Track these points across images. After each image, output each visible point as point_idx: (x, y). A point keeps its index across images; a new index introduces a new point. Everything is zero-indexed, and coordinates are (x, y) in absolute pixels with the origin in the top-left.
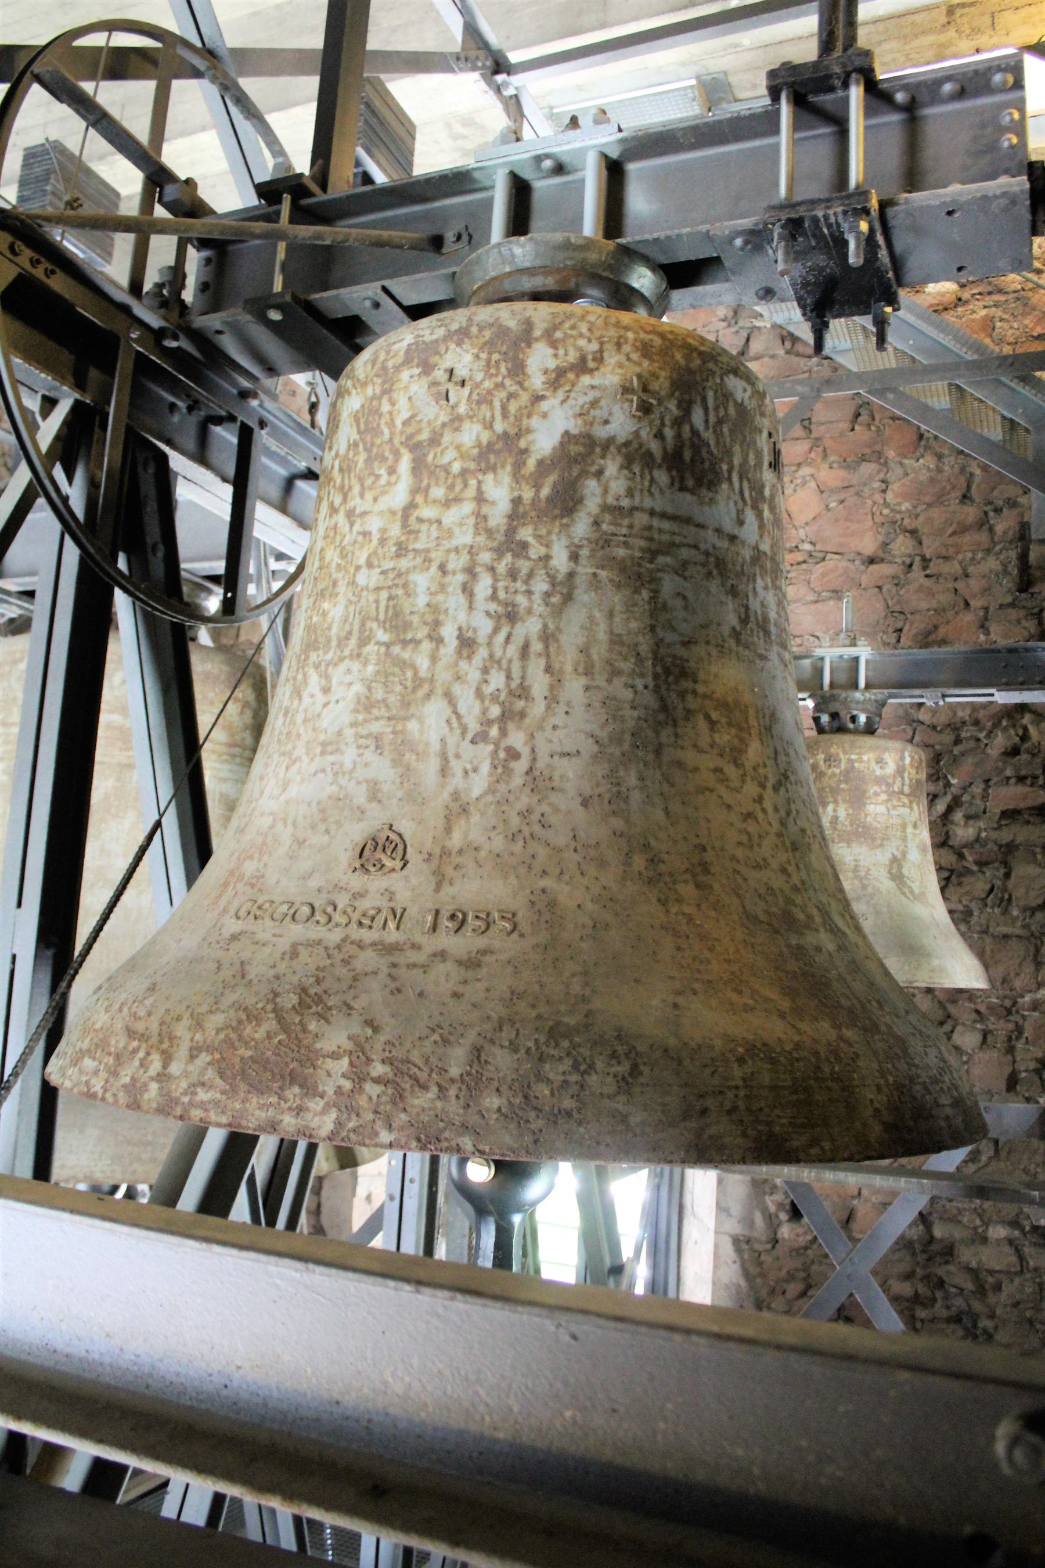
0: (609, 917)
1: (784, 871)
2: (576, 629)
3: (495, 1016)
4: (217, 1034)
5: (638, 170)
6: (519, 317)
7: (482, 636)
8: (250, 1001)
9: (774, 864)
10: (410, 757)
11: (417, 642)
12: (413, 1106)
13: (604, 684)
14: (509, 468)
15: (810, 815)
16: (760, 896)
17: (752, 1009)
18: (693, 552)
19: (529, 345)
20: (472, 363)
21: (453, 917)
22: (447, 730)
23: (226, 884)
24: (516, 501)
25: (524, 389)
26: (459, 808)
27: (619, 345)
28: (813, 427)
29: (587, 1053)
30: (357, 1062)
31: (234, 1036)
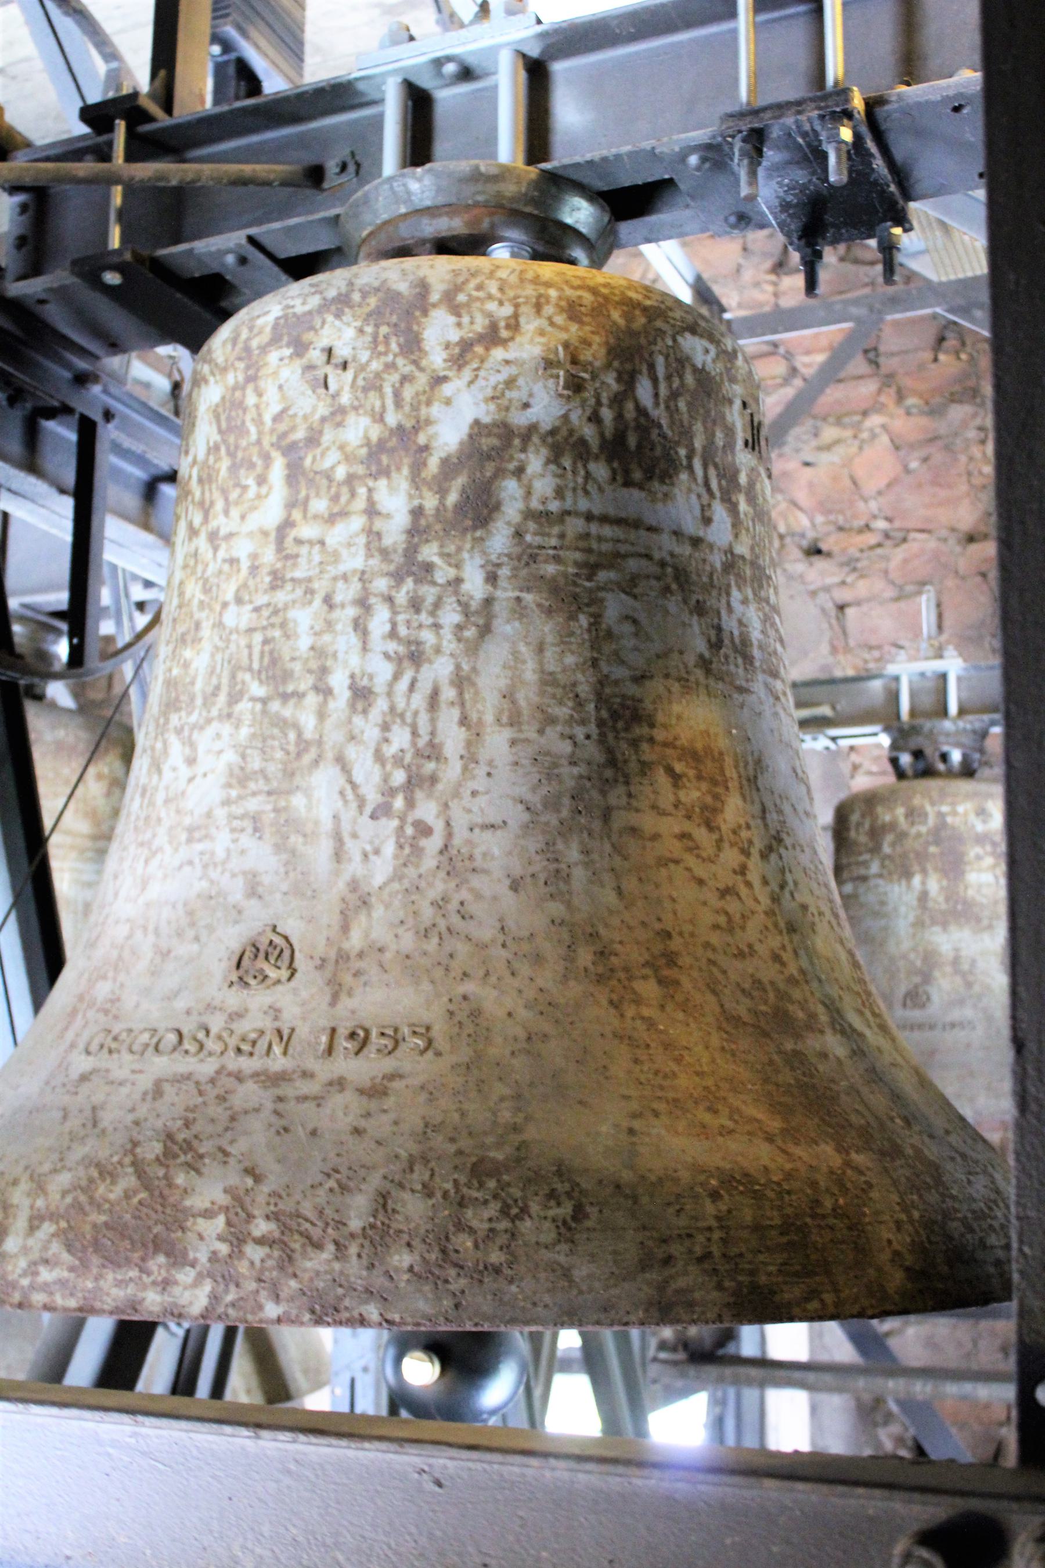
0: (547, 1027)
1: (776, 958)
2: (497, 670)
3: (403, 1154)
4: (63, 1197)
5: (569, 70)
6: (411, 277)
7: (380, 685)
8: (103, 1154)
9: (761, 949)
10: (295, 840)
11: (300, 696)
12: (305, 1270)
13: (533, 735)
14: (405, 471)
15: (814, 885)
16: (743, 991)
17: (731, 1132)
18: (644, 562)
19: (425, 313)
20: (355, 339)
21: (353, 1035)
22: (340, 803)
23: (74, 1012)
24: (417, 513)
25: (422, 369)
26: (358, 900)
27: (538, 307)
28: (882, 360)
29: (516, 1192)
30: (234, 1219)
31: (83, 1198)
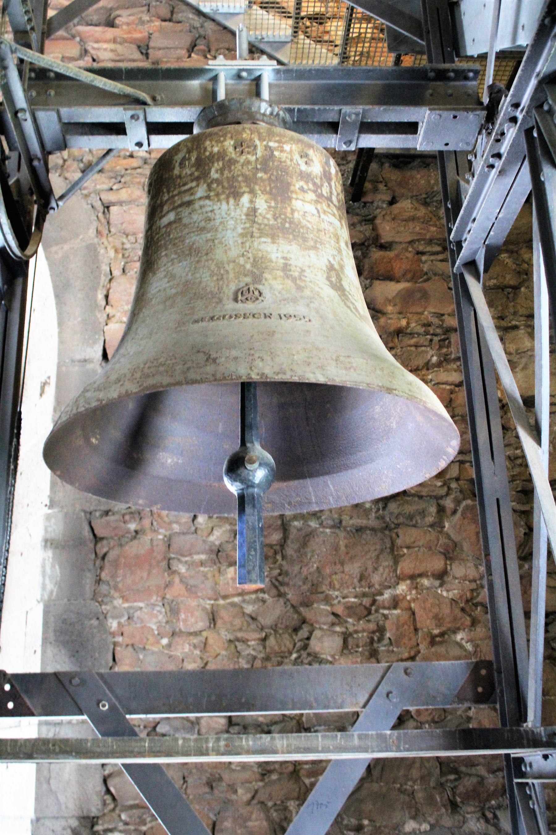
28: (150, 51)
